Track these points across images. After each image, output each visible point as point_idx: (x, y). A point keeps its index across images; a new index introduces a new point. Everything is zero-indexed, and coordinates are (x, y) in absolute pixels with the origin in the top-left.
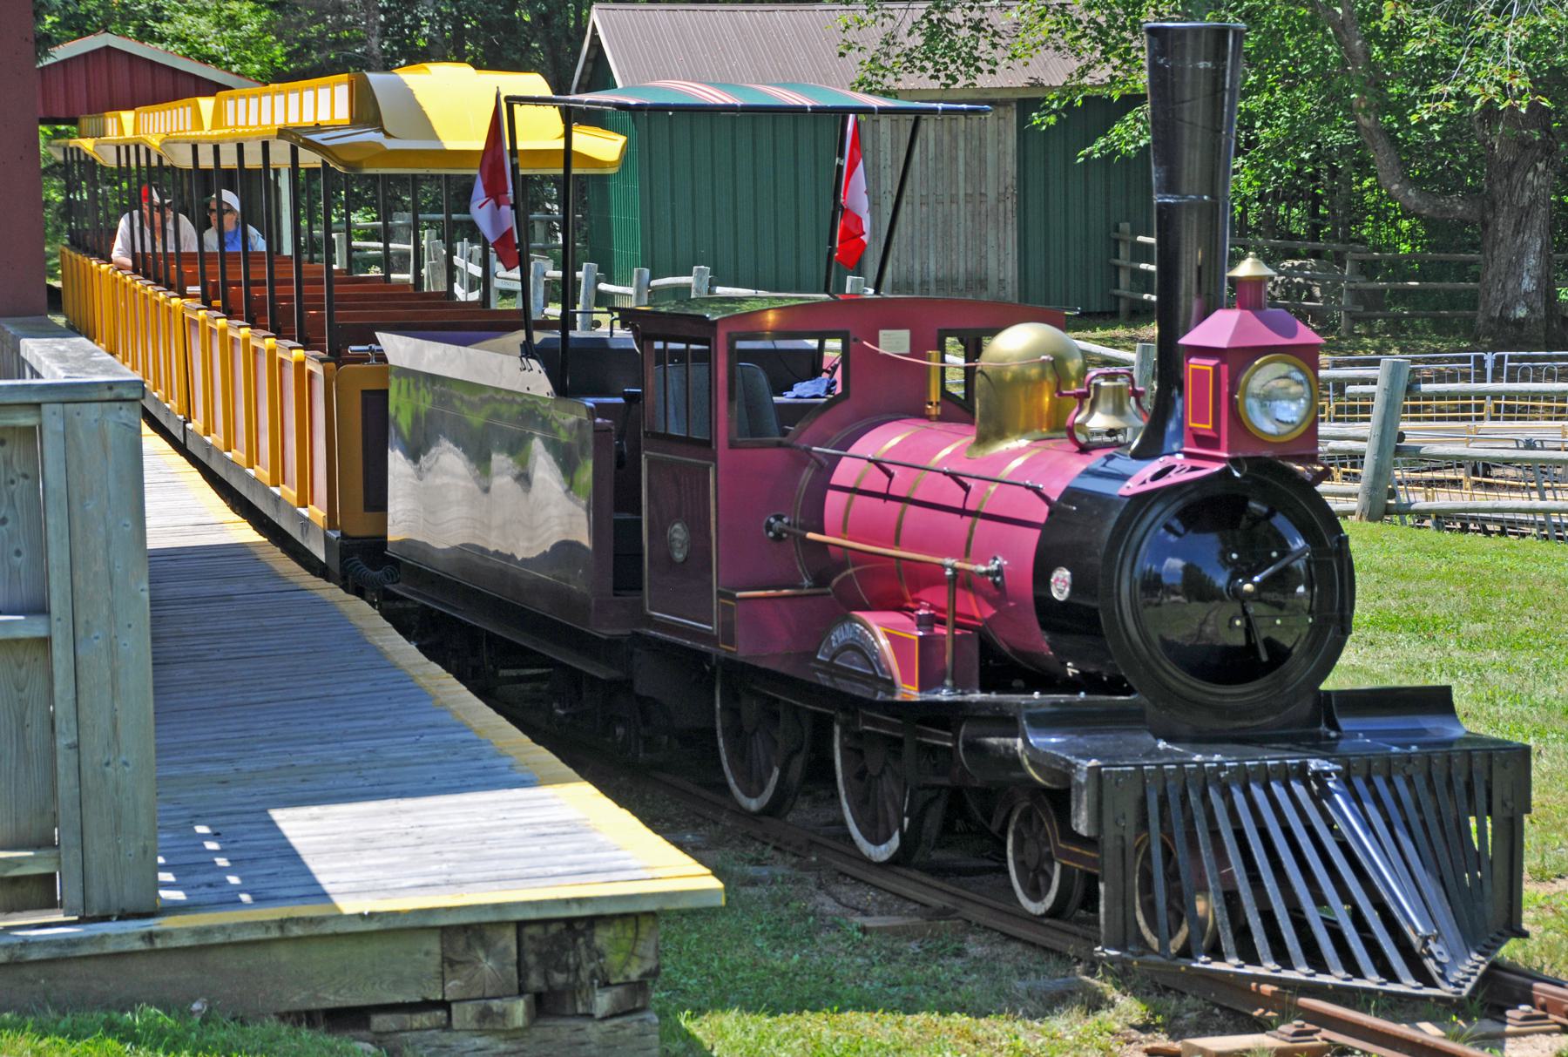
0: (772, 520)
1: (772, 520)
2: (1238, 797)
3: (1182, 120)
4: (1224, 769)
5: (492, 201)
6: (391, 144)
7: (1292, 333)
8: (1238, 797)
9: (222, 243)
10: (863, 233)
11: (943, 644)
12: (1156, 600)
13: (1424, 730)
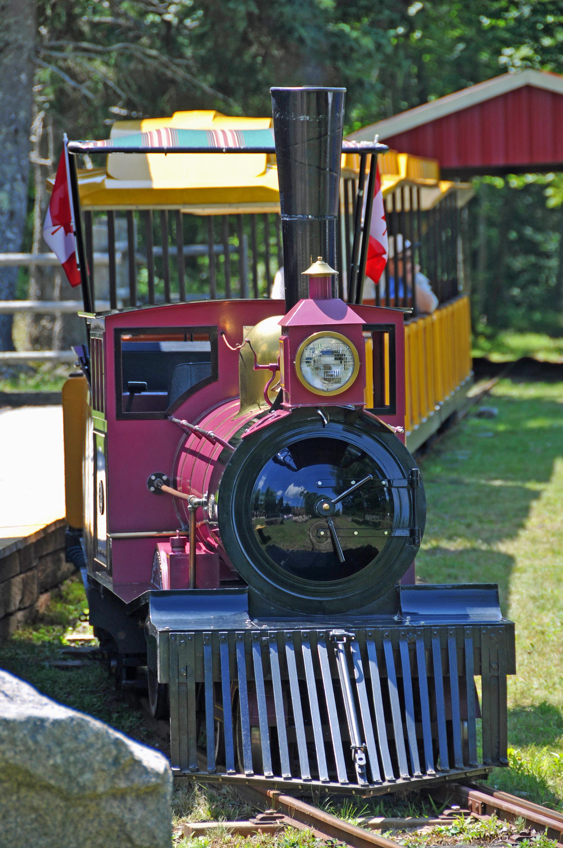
0: (153, 478)
1: (153, 478)
2: (274, 656)
3: (296, 161)
4: (266, 635)
5: (62, 229)
6: (110, 184)
7: (343, 315)
8: (274, 656)
9: (227, 283)
10: (384, 252)
11: (187, 562)
12: (280, 519)
13: (468, 615)
